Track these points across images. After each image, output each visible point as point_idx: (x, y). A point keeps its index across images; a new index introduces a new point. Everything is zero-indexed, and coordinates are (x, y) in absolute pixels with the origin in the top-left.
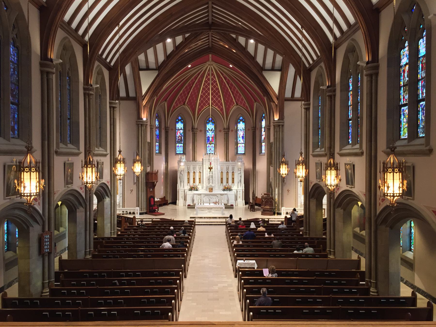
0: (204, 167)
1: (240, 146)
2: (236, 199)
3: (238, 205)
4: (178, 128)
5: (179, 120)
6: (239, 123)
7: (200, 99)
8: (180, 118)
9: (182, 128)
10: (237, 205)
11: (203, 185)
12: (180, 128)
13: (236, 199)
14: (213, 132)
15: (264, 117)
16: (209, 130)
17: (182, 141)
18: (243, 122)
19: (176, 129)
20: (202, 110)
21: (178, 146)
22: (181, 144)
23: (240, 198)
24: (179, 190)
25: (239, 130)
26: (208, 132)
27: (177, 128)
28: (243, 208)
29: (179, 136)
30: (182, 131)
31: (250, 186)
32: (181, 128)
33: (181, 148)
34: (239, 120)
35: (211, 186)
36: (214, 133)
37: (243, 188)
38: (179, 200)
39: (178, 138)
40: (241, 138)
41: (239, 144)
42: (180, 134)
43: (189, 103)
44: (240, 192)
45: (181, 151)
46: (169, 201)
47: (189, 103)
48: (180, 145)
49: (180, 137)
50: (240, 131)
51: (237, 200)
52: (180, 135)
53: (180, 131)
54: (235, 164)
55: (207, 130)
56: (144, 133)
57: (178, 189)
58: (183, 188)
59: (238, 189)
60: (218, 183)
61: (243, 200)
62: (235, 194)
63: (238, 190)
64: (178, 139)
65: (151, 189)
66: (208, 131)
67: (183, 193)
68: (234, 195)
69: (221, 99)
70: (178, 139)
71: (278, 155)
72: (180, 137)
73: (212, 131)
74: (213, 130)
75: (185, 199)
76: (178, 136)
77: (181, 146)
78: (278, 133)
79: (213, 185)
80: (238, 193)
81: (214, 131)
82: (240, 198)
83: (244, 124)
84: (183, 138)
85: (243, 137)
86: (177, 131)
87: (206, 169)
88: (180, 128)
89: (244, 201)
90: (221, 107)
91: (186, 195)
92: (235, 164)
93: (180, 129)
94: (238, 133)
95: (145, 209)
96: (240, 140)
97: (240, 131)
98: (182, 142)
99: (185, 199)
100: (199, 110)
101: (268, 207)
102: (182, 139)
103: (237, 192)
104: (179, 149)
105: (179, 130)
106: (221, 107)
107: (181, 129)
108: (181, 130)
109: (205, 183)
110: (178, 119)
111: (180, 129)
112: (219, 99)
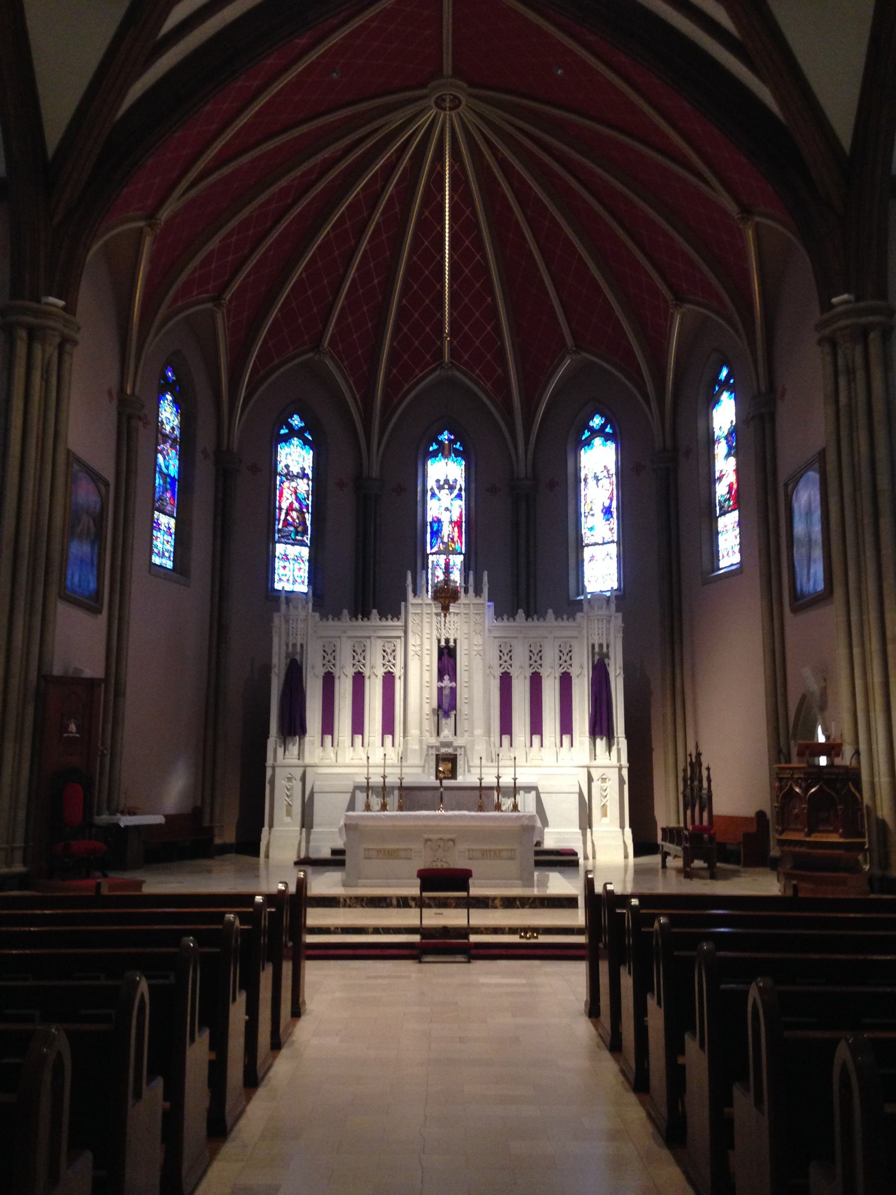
0: (411, 648)
1: (592, 559)
2: (586, 822)
3: (597, 856)
4: (287, 466)
5: (294, 433)
6: (588, 443)
7: (397, 329)
8: (296, 421)
9: (309, 471)
10: (590, 856)
11: (406, 743)
12: (295, 469)
13: (586, 822)
14: (459, 496)
15: (725, 385)
16: (440, 488)
17: (304, 532)
18: (606, 440)
19: (276, 473)
20: (406, 387)
21: (286, 557)
22: (297, 548)
23: (605, 815)
24: (278, 770)
25: (585, 480)
26: (433, 495)
27: (281, 467)
28: (626, 867)
29: (291, 508)
30: (304, 486)
31: (654, 754)
32: (303, 469)
33: (297, 566)
34: (587, 434)
35: (448, 745)
36: (462, 503)
37: (619, 760)
38: (271, 826)
39: (287, 514)
40: (600, 515)
41: (588, 545)
42: (297, 499)
43: (340, 347)
44: (604, 780)
45: (299, 580)
46: (228, 835)
47: (340, 347)
48: (293, 551)
49: (296, 510)
50: (591, 482)
51: (591, 827)
52: (296, 505)
53: (294, 484)
54: (575, 634)
55: (432, 489)
56: (46, 380)
57: (269, 762)
58: (295, 762)
59: (594, 763)
60: (488, 732)
61: (622, 827)
62: (581, 794)
63: (592, 771)
64: (286, 523)
65: (73, 728)
66: (437, 491)
67: (297, 785)
68: (577, 796)
69: (497, 328)
70: (286, 520)
71: (867, 506)
72: (294, 514)
73: (456, 492)
74: (460, 489)
75: (307, 822)
76: (285, 505)
77: (298, 559)
78: (860, 375)
79: (459, 741)
80: (594, 785)
81: (463, 493)
82: (605, 815)
83: (611, 447)
84: (308, 517)
85: (607, 511)
86: (282, 482)
87: (421, 657)
88: (295, 469)
89: (628, 831)
90: (500, 371)
91: (312, 793)
92: (575, 634)
93: (297, 477)
94: (583, 493)
95: (19, 855)
96: (591, 529)
97: (591, 482)
98: (307, 539)
99: (307, 822)
100: (392, 386)
101: (834, 838)
102: (303, 522)
103: (590, 779)
104: (286, 571)
105: (290, 476)
106: (500, 371)
107: (304, 476)
108: (299, 481)
109: (414, 731)
110: (290, 426)
111: (297, 477)
112: (489, 328)
